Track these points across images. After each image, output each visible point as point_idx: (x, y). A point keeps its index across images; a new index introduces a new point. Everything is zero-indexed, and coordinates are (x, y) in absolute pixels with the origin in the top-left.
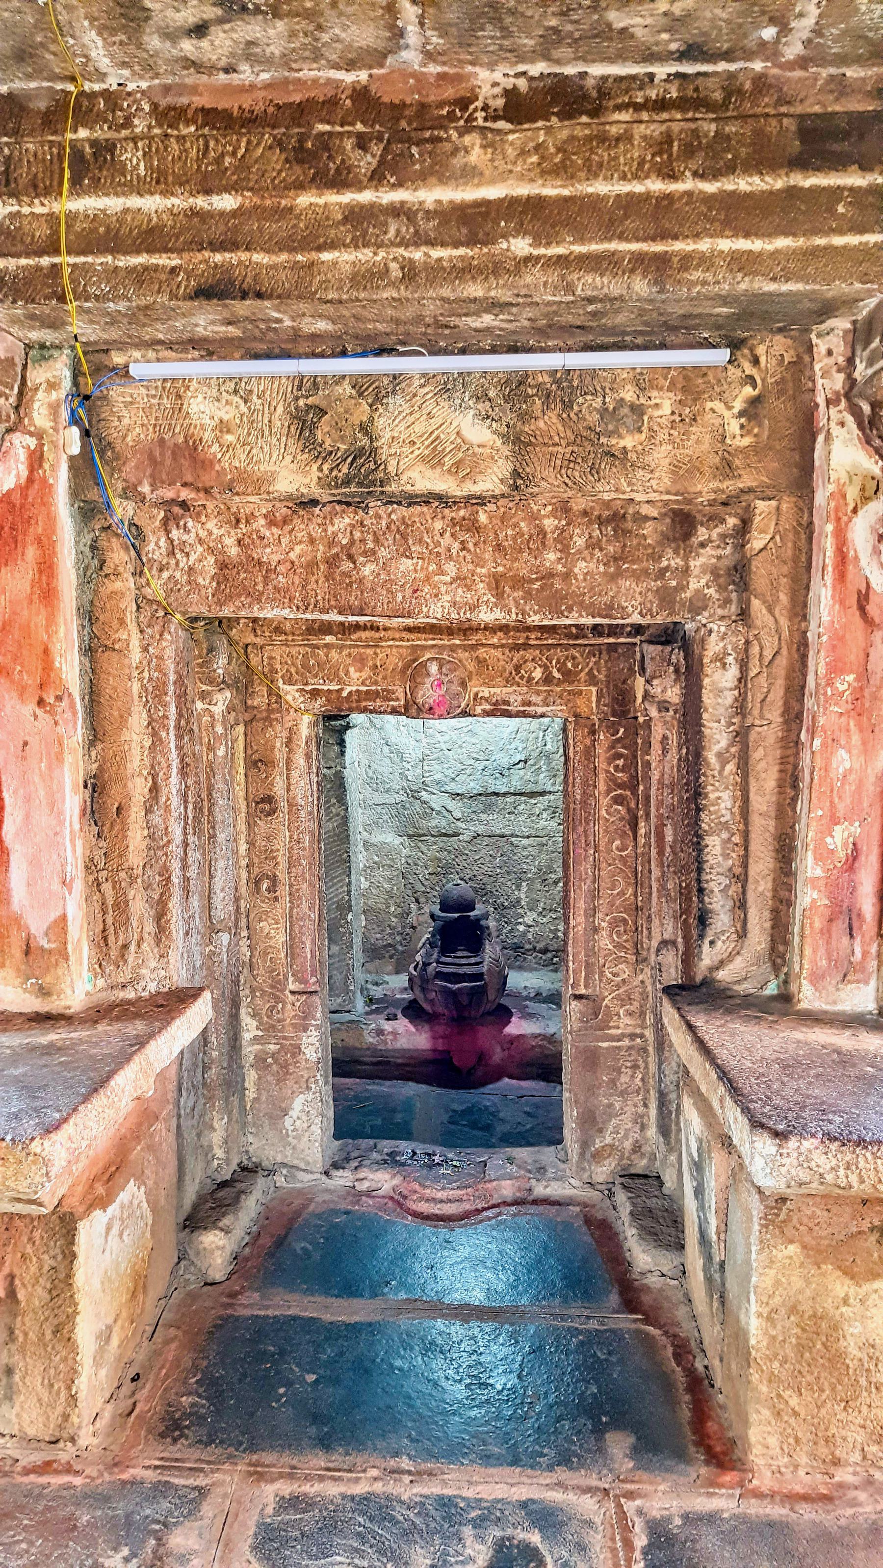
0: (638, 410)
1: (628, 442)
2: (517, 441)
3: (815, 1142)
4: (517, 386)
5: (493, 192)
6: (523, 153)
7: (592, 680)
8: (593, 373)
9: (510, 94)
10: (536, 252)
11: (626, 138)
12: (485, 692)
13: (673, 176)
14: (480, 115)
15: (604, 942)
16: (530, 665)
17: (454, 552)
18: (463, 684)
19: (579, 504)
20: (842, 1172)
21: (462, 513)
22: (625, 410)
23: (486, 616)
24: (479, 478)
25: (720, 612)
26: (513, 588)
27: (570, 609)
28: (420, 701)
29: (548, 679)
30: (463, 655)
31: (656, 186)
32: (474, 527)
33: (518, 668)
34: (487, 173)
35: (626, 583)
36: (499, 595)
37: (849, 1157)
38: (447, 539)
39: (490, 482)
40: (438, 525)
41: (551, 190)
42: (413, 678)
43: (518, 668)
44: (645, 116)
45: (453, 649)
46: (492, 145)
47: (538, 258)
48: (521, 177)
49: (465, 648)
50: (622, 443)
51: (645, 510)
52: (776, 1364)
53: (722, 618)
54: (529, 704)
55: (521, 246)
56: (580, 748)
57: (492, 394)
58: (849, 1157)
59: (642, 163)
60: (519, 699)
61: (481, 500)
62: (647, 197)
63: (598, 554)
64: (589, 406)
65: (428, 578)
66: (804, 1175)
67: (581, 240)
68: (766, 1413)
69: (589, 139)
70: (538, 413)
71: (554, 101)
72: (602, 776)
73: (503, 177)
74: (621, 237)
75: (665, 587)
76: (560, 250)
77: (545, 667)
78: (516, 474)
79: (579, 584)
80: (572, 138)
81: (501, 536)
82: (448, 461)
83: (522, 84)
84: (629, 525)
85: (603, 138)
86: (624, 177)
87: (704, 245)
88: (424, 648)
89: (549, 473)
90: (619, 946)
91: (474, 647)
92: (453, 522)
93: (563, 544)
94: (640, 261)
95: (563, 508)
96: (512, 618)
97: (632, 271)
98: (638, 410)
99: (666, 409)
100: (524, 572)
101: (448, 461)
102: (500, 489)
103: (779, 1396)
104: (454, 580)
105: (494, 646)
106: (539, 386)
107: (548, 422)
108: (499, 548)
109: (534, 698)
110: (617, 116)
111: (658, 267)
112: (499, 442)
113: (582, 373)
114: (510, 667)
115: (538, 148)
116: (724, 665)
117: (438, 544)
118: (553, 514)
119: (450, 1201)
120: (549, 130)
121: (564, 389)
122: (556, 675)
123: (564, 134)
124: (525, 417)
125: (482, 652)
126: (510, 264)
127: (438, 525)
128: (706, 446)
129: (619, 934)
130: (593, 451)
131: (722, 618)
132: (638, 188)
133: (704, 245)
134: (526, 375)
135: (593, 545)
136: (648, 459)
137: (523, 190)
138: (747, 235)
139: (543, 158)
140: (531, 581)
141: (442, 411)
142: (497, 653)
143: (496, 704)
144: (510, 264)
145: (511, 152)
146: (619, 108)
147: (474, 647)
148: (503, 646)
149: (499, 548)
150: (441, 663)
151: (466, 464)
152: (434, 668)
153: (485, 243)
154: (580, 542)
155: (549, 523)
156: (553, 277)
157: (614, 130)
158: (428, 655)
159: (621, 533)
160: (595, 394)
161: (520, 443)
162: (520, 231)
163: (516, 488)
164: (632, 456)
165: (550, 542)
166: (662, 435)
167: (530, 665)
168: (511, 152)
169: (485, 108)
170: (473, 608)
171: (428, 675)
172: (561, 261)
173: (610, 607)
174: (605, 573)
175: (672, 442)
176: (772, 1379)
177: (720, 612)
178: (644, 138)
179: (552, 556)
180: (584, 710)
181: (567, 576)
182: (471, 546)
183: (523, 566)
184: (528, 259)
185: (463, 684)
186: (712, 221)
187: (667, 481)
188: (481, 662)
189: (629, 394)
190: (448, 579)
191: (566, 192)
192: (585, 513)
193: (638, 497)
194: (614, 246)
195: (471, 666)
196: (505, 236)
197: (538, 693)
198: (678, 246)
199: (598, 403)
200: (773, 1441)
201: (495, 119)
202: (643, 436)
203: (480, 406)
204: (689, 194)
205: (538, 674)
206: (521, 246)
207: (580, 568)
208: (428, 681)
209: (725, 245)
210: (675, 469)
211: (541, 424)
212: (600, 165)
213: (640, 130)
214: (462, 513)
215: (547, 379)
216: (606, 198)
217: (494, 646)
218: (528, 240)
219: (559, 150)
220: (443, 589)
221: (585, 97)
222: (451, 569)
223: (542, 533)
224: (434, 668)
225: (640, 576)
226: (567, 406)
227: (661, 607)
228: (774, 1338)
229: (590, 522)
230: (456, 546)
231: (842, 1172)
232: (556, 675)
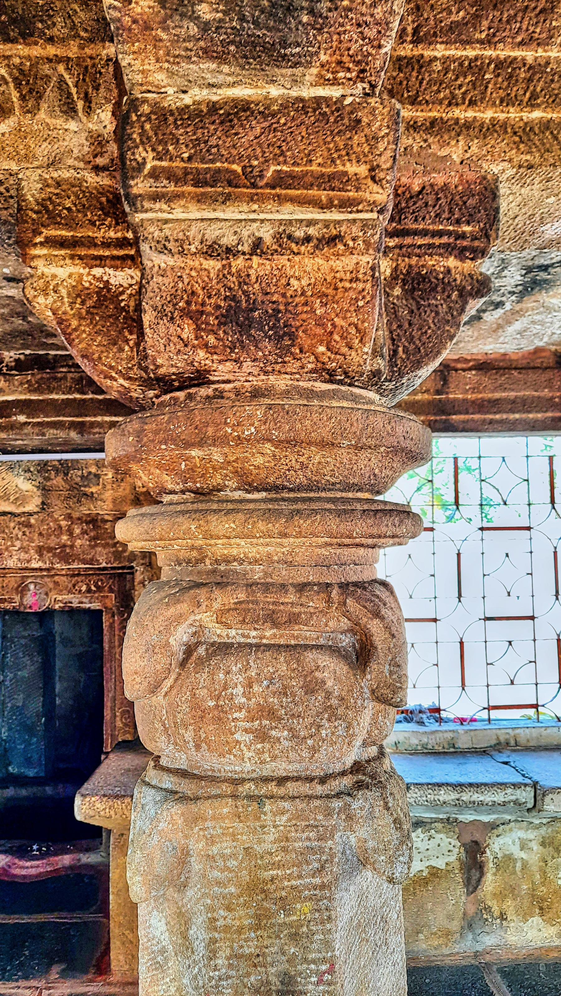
0: (97, 476)
1: (94, 489)
2: (44, 489)
3: (97, 798)
4: (43, 466)
5: (10, 398)
6: (21, 384)
7: (111, 590)
8: (77, 461)
9: (17, 361)
10: (29, 420)
11: (65, 378)
12: (60, 598)
13: (84, 393)
14: (5, 369)
15: (119, 724)
16: (80, 584)
17: (19, 536)
18: (47, 594)
19: (76, 515)
20: (107, 810)
21: (23, 519)
22: (92, 476)
23: (34, 565)
24: (26, 505)
25: (142, 561)
26: (48, 552)
27: (74, 561)
28: (25, 603)
29: (89, 591)
30: (47, 580)
31: (78, 396)
32: (29, 525)
33: (74, 586)
34: (7, 391)
35: (99, 549)
36: (41, 555)
37: (111, 803)
38: (16, 531)
39: (31, 507)
40: (12, 525)
41: (34, 397)
42: (22, 592)
43: (74, 586)
44: (73, 370)
45: (42, 577)
46: (8, 380)
47: (30, 423)
48: (21, 393)
49: (48, 576)
50: (91, 490)
51: (106, 517)
52: (121, 918)
53: (142, 564)
54: (82, 603)
55: (22, 418)
56: (108, 624)
57: (32, 469)
58: (111, 803)
59: (71, 388)
60: (77, 600)
61: (31, 514)
62: (75, 399)
63: (86, 537)
64: (76, 475)
65: (7, 549)
66: (92, 813)
67: (47, 416)
68: (118, 943)
69: (48, 379)
70: (53, 477)
71: (36, 364)
72: (117, 637)
73: (13, 392)
74: (64, 416)
75: (117, 551)
76: (39, 420)
77: (88, 585)
78: (43, 503)
79: (77, 550)
80: (42, 378)
81: (42, 529)
82: (12, 498)
83: (22, 357)
84: (99, 524)
85: (55, 378)
86: (63, 393)
87: (99, 419)
88: (28, 577)
89: (58, 502)
90: (126, 725)
91: (53, 576)
92: (19, 523)
93: (70, 532)
94: (73, 425)
95: (69, 517)
96: (47, 566)
97: (69, 428)
98: (97, 476)
99: (110, 476)
100: (52, 545)
101: (12, 498)
102: (36, 509)
103: (123, 934)
104: (19, 549)
105: (63, 575)
106: (54, 466)
107: (58, 481)
108: (40, 534)
109: (84, 600)
110: (61, 370)
111: (81, 427)
112: (35, 489)
113: (72, 461)
114: (70, 585)
115: (28, 382)
116: (144, 586)
117: (12, 533)
118: (64, 519)
119: (32, 867)
120: (33, 375)
121: (64, 468)
122: (93, 588)
123: (39, 376)
124: (48, 479)
125: (56, 578)
126: (18, 425)
127: (12, 525)
128: (127, 491)
129: (126, 719)
130: (78, 493)
131: (142, 564)
132: (71, 397)
133: (99, 419)
134: (48, 461)
135: (84, 532)
136: (103, 497)
137: (23, 397)
138: (115, 416)
139: (30, 385)
140: (56, 549)
141: (9, 477)
142: (64, 579)
143: (66, 603)
144: (18, 425)
145: (16, 383)
146: (62, 366)
147: (53, 576)
148: (67, 575)
149: (40, 534)
150: (36, 584)
151: (21, 499)
152: (32, 587)
153: (6, 417)
154: (77, 531)
155: (63, 523)
156: (36, 430)
157: (59, 375)
158: (30, 580)
159: (96, 527)
160: (78, 469)
161: (45, 490)
162: (22, 413)
163: (44, 509)
164: (96, 495)
165: (64, 532)
166: (109, 487)
167: (80, 584)
168: (16, 383)
169: (7, 366)
170: (28, 562)
171: (29, 590)
172: (39, 424)
173: (92, 560)
174: (90, 545)
175: (113, 489)
176: (120, 925)
177: (142, 561)
178: (72, 378)
179: (65, 538)
180: (109, 605)
181: (72, 547)
182: (27, 533)
183: (53, 542)
184: (26, 423)
185: (47, 594)
186: (101, 410)
187: (111, 506)
188: (56, 583)
189: (93, 470)
190: (16, 548)
191: (41, 398)
192: (79, 519)
193: (101, 513)
194: (61, 418)
195: (51, 585)
196: (15, 415)
197: (86, 597)
198: (88, 419)
199: (80, 473)
200: (121, 957)
201: (11, 370)
202: (100, 487)
203: (27, 474)
204: (91, 399)
205: (84, 588)
206: (22, 418)
207: (78, 542)
208: (29, 594)
209: (107, 419)
210: (114, 501)
211: (54, 482)
212: (54, 388)
213: (70, 375)
214: (23, 519)
215: (57, 463)
216: (58, 400)
217: (63, 575)
218: (25, 416)
219: (37, 382)
220: (14, 553)
221: (49, 362)
222: (18, 544)
223: (60, 527)
224: (32, 587)
225: (105, 546)
226: (66, 474)
227: (115, 560)
228: (120, 904)
229: (82, 523)
230: (21, 533)
231: (107, 810)
232: (93, 588)
